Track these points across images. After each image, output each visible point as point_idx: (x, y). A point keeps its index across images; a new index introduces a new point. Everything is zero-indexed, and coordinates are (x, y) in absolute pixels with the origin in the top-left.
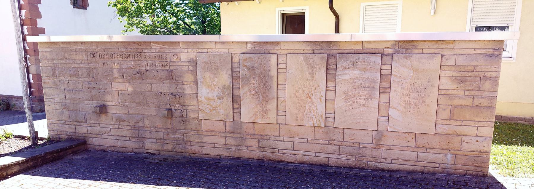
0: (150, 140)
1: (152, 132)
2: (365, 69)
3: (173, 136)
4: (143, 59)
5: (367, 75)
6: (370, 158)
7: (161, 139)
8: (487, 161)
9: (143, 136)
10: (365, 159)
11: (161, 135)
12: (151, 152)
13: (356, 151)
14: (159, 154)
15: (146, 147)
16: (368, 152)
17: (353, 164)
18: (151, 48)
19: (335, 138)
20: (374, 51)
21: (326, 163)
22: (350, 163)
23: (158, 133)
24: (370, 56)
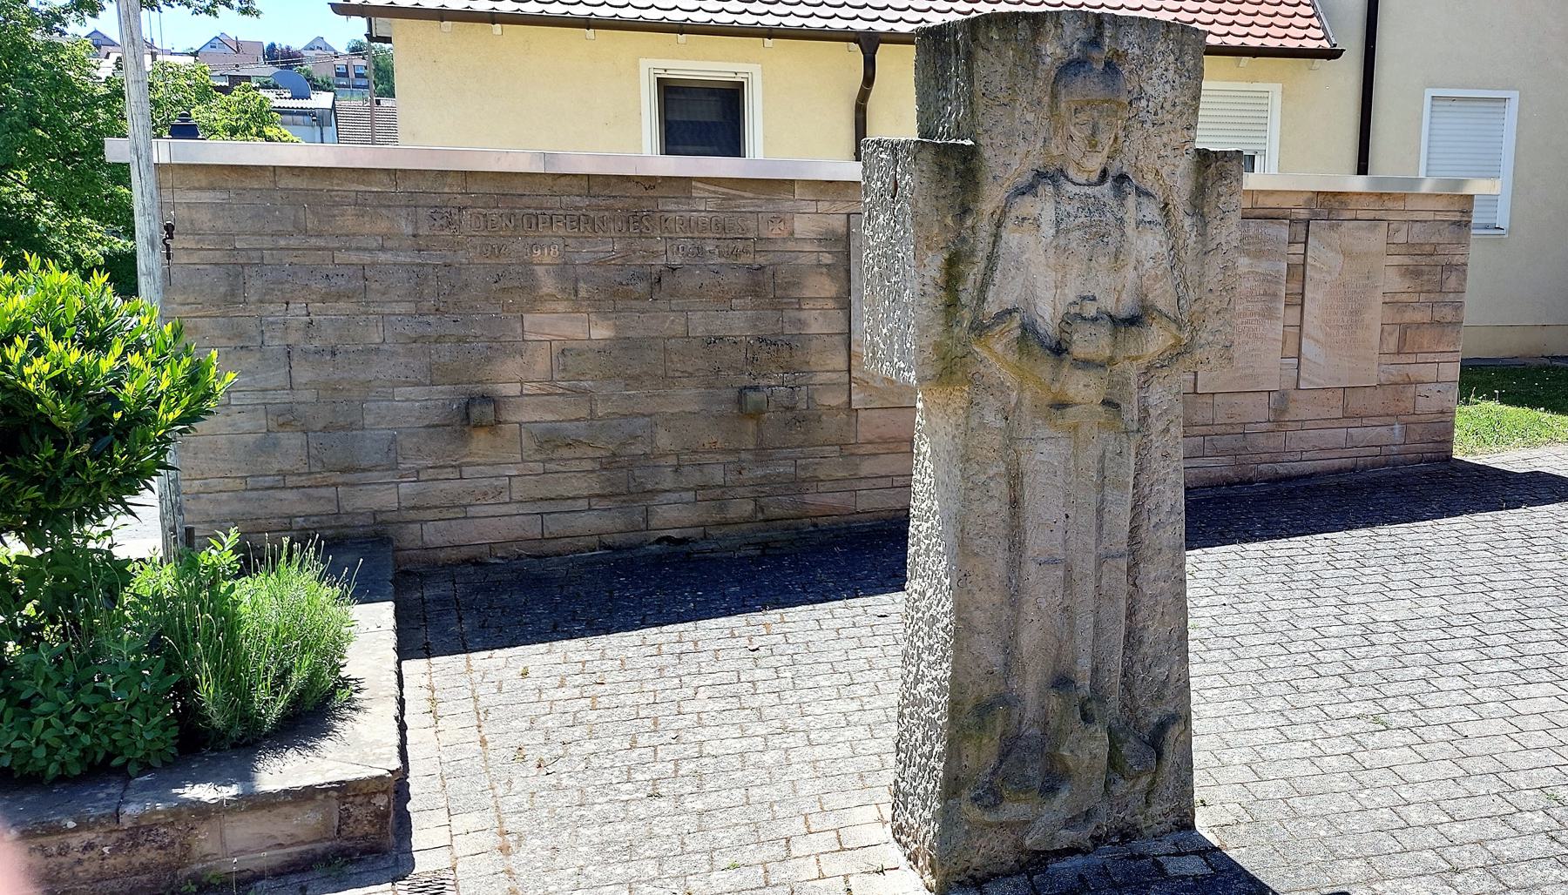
0: (674, 496)
1: (685, 470)
2: (1259, 254)
3: (760, 473)
5: (1264, 266)
8: (1154, 738)
9: (649, 487)
10: (1256, 458)
11: (718, 475)
12: (674, 534)
14: (705, 537)
15: (653, 523)
16: (1262, 441)
23: (706, 470)
24: (1268, 223)
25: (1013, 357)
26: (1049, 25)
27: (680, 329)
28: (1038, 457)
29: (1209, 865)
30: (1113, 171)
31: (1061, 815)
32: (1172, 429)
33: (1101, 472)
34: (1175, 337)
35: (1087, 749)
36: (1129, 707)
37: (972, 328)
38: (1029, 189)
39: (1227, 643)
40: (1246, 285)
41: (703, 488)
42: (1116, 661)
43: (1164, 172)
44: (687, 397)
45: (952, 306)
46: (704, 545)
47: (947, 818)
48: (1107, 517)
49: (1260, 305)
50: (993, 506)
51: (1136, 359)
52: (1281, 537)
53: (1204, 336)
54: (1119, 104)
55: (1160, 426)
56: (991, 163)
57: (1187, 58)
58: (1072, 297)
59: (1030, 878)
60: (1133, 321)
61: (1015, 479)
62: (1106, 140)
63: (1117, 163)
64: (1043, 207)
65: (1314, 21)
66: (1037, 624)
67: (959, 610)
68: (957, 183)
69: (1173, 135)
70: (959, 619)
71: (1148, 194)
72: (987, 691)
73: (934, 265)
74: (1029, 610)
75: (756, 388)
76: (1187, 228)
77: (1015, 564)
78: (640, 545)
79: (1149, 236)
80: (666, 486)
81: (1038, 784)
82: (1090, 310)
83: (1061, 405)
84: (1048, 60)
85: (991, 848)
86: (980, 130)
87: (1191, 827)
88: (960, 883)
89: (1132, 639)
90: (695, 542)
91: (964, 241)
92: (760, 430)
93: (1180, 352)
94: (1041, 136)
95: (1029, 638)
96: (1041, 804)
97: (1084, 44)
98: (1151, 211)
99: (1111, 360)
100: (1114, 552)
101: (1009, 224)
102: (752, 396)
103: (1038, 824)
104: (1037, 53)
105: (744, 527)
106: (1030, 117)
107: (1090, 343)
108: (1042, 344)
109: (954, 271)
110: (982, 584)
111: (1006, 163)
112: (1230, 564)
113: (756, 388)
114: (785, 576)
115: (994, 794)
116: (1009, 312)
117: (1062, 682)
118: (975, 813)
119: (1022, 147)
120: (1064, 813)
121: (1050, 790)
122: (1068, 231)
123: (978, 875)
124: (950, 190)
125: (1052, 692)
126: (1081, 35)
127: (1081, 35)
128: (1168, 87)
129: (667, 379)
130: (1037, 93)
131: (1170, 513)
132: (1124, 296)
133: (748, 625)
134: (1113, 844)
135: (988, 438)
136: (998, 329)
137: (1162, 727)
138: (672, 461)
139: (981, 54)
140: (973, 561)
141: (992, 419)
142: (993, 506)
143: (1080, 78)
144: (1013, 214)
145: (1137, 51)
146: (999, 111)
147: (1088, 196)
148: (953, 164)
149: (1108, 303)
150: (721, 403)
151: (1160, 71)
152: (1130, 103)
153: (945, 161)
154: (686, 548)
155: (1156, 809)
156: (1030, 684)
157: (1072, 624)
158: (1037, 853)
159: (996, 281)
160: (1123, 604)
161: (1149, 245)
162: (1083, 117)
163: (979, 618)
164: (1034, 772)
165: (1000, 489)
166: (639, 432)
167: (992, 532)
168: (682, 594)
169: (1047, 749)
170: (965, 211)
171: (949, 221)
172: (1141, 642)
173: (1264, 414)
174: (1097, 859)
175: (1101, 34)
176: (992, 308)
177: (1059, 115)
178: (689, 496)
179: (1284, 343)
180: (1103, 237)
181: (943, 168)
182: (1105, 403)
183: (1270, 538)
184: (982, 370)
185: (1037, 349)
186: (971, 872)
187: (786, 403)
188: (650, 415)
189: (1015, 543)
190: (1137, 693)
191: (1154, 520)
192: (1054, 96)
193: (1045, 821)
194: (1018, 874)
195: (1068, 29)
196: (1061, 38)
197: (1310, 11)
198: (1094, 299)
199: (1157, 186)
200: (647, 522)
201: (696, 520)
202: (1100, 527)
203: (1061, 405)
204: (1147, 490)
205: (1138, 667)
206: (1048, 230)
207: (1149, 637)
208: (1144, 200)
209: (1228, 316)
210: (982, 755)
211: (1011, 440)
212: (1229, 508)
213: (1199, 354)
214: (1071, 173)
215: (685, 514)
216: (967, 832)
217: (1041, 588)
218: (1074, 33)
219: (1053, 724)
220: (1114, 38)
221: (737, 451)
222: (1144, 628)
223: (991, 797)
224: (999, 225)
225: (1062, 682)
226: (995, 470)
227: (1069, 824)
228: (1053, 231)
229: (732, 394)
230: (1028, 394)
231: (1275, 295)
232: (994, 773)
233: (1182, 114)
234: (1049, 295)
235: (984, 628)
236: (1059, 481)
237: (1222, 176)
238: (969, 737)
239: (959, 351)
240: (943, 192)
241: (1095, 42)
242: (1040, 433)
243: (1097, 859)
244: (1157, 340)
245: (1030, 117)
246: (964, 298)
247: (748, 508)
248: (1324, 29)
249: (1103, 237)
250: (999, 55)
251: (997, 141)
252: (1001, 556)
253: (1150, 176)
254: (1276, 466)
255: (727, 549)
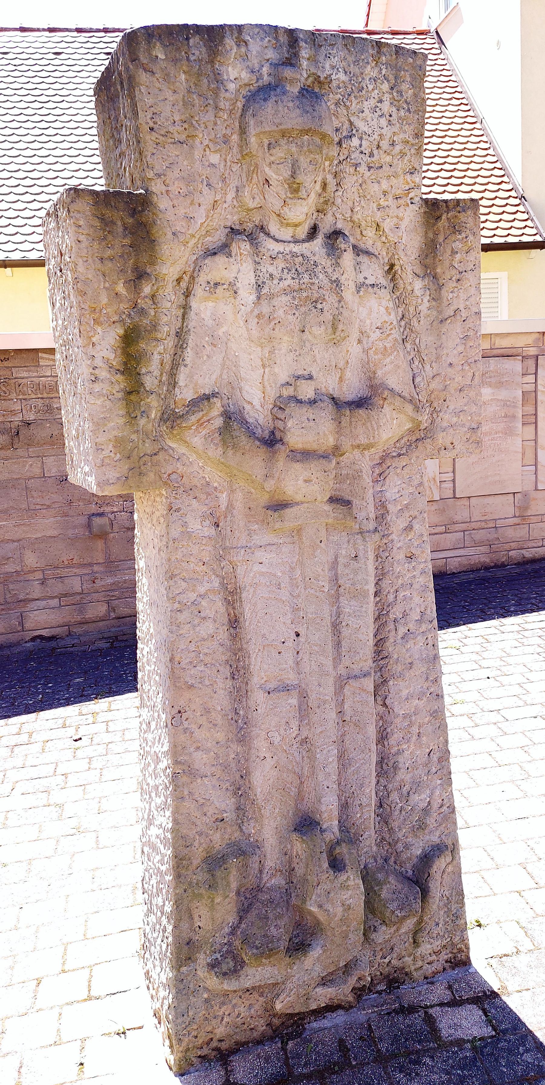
0: (42, 604)
1: (50, 582)
2: (500, 385)
3: (110, 580)
4: (13, 395)
5: (503, 394)
6: (512, 544)
7: (74, 594)
8: (415, 875)
9: (21, 597)
10: (507, 547)
11: (76, 585)
12: (45, 633)
13: (493, 536)
14: (69, 634)
15: (28, 625)
16: (511, 533)
17: (485, 559)
18: (38, 366)
19: (458, 518)
20: (509, 352)
21: (443, 569)
22: (482, 560)
23: (66, 581)
24: (505, 360)
25: (215, 452)
26: (229, 42)
27: (37, 471)
28: (257, 568)
29: (489, 1022)
30: (326, 226)
31: (315, 974)
32: (416, 526)
33: (335, 580)
34: (413, 420)
35: (338, 901)
36: (387, 840)
37: (163, 419)
38: (224, 249)
39: (494, 717)
40: (491, 409)
41: (66, 595)
42: (368, 796)
43: (387, 225)
44: (47, 525)
45: (133, 392)
46: (69, 641)
47: (182, 987)
48: (345, 632)
49: (502, 425)
50: (207, 628)
51: (368, 447)
52: (532, 611)
53: (446, 418)
54: (324, 136)
55: (402, 523)
56: (170, 215)
57: (404, 87)
58: (284, 377)
59: (284, 1044)
60: (360, 403)
61: (232, 595)
62: (310, 183)
63: (329, 219)
64: (239, 268)
65: (529, 223)
66: (270, 762)
67: (176, 752)
68: (127, 241)
69: (394, 181)
70: (176, 762)
71: (367, 253)
72: (219, 840)
73: (107, 341)
74: (260, 745)
75: (101, 515)
76: (418, 292)
77: (240, 694)
78: (18, 644)
79: (372, 302)
80: (35, 596)
81: (283, 944)
82: (307, 391)
83: (279, 506)
84: (232, 87)
85: (235, 1012)
86: (150, 174)
87: (466, 963)
88: (203, 1058)
89: (386, 767)
90: (62, 638)
91: (142, 312)
92: (107, 547)
93: (419, 437)
94: (234, 183)
95: (263, 778)
96: (290, 965)
97: (275, 66)
98: (374, 272)
99: (337, 451)
100: (357, 672)
101: (199, 291)
102: (97, 521)
103: (289, 985)
104: (218, 79)
105: (101, 624)
106: (215, 158)
107: (307, 430)
108: (251, 434)
109: (132, 350)
110: (203, 721)
111: (187, 216)
112: (491, 638)
113: (101, 515)
114: (122, 666)
115: (234, 958)
116: (207, 398)
117: (306, 824)
118: (213, 982)
119: (207, 197)
120: (318, 971)
121: (298, 947)
122: (271, 296)
123: (224, 1046)
124: (118, 250)
125: (295, 836)
126: (271, 54)
127: (271, 54)
128: (383, 122)
129: (31, 512)
130: (221, 130)
131: (420, 621)
132: (348, 374)
133: (81, 714)
134: (379, 993)
135: (195, 550)
136: (193, 418)
137: (427, 860)
138: (39, 575)
139: (143, 77)
140: (187, 695)
141: (199, 527)
142: (207, 628)
143: (270, 103)
144: (202, 278)
145: (342, 76)
146: (173, 151)
147: (294, 255)
148: (120, 217)
149: (330, 384)
150: (75, 527)
151: (372, 102)
152: (340, 143)
153: (108, 213)
154: (53, 644)
155: (426, 948)
156: (269, 829)
157: (312, 758)
158: (291, 1015)
159: (188, 360)
160: (372, 731)
161: (373, 311)
162: (279, 153)
163: (201, 760)
164: (280, 930)
165: (215, 608)
166: (10, 555)
167: (208, 659)
168: (35, 687)
169: (294, 901)
170: (140, 276)
171: (120, 288)
172: (396, 768)
173: (510, 511)
174: (361, 1016)
175: (296, 55)
176: (186, 393)
177: (250, 154)
178: (55, 602)
179: (523, 454)
180: (314, 301)
181: (106, 223)
182: (333, 500)
183: (523, 612)
184: (181, 469)
185: (244, 440)
186: (214, 1044)
187: (127, 525)
188: (19, 541)
189: (238, 670)
190: (395, 825)
191: (402, 630)
192: (243, 131)
193: (299, 983)
194: (271, 1039)
195: (255, 47)
196: (245, 58)
197: (525, 216)
198: (310, 378)
199: (379, 244)
200: (22, 624)
201: (61, 621)
202: (338, 645)
203: (279, 506)
204: (391, 598)
205: (395, 796)
206: (247, 296)
207: (404, 761)
208: (364, 259)
209: (472, 394)
210: (217, 914)
211: (223, 552)
212: (487, 588)
213: (442, 439)
214: (273, 228)
215: (52, 616)
216: (207, 1001)
217: (272, 720)
218: (262, 53)
219: (300, 871)
220: (313, 60)
221: (91, 565)
222: (399, 753)
223: (229, 962)
224: (187, 294)
225: (306, 824)
226: (207, 586)
227: (324, 982)
228: (253, 297)
229: (83, 520)
230: (239, 495)
231: (514, 417)
232: (233, 932)
233: (403, 154)
234: (256, 376)
235: (208, 770)
236: (284, 594)
237: (455, 229)
238: (199, 897)
239: (148, 447)
240: (109, 253)
241: (290, 61)
242: (258, 539)
243: (361, 1016)
244: (390, 424)
245: (215, 158)
246: (149, 382)
247: (102, 609)
248: (537, 228)
249: (314, 301)
250: (167, 77)
251: (174, 189)
252: (223, 685)
253: (370, 233)
254: (523, 552)
255: (85, 644)
